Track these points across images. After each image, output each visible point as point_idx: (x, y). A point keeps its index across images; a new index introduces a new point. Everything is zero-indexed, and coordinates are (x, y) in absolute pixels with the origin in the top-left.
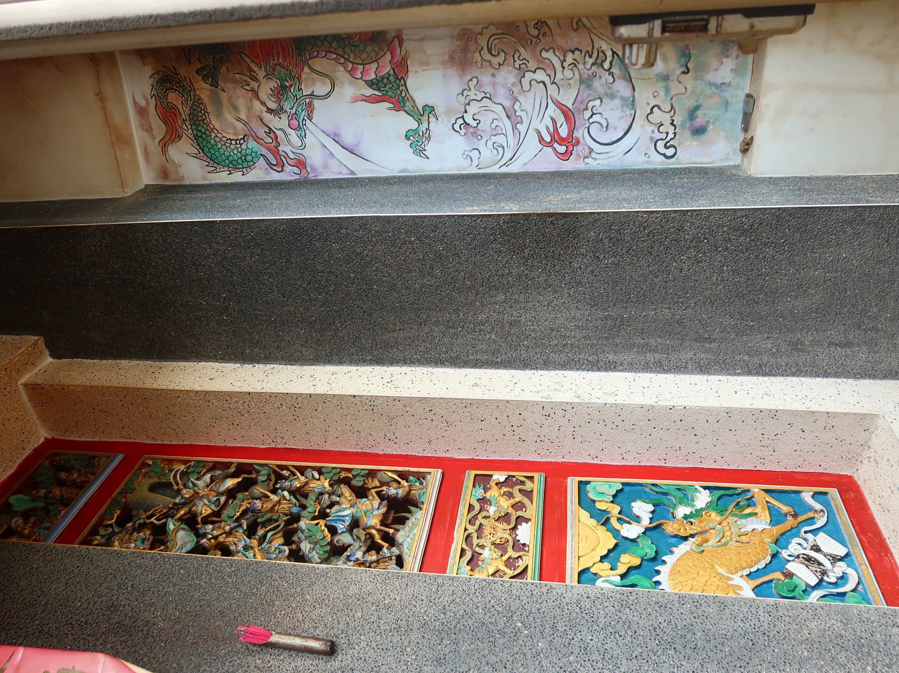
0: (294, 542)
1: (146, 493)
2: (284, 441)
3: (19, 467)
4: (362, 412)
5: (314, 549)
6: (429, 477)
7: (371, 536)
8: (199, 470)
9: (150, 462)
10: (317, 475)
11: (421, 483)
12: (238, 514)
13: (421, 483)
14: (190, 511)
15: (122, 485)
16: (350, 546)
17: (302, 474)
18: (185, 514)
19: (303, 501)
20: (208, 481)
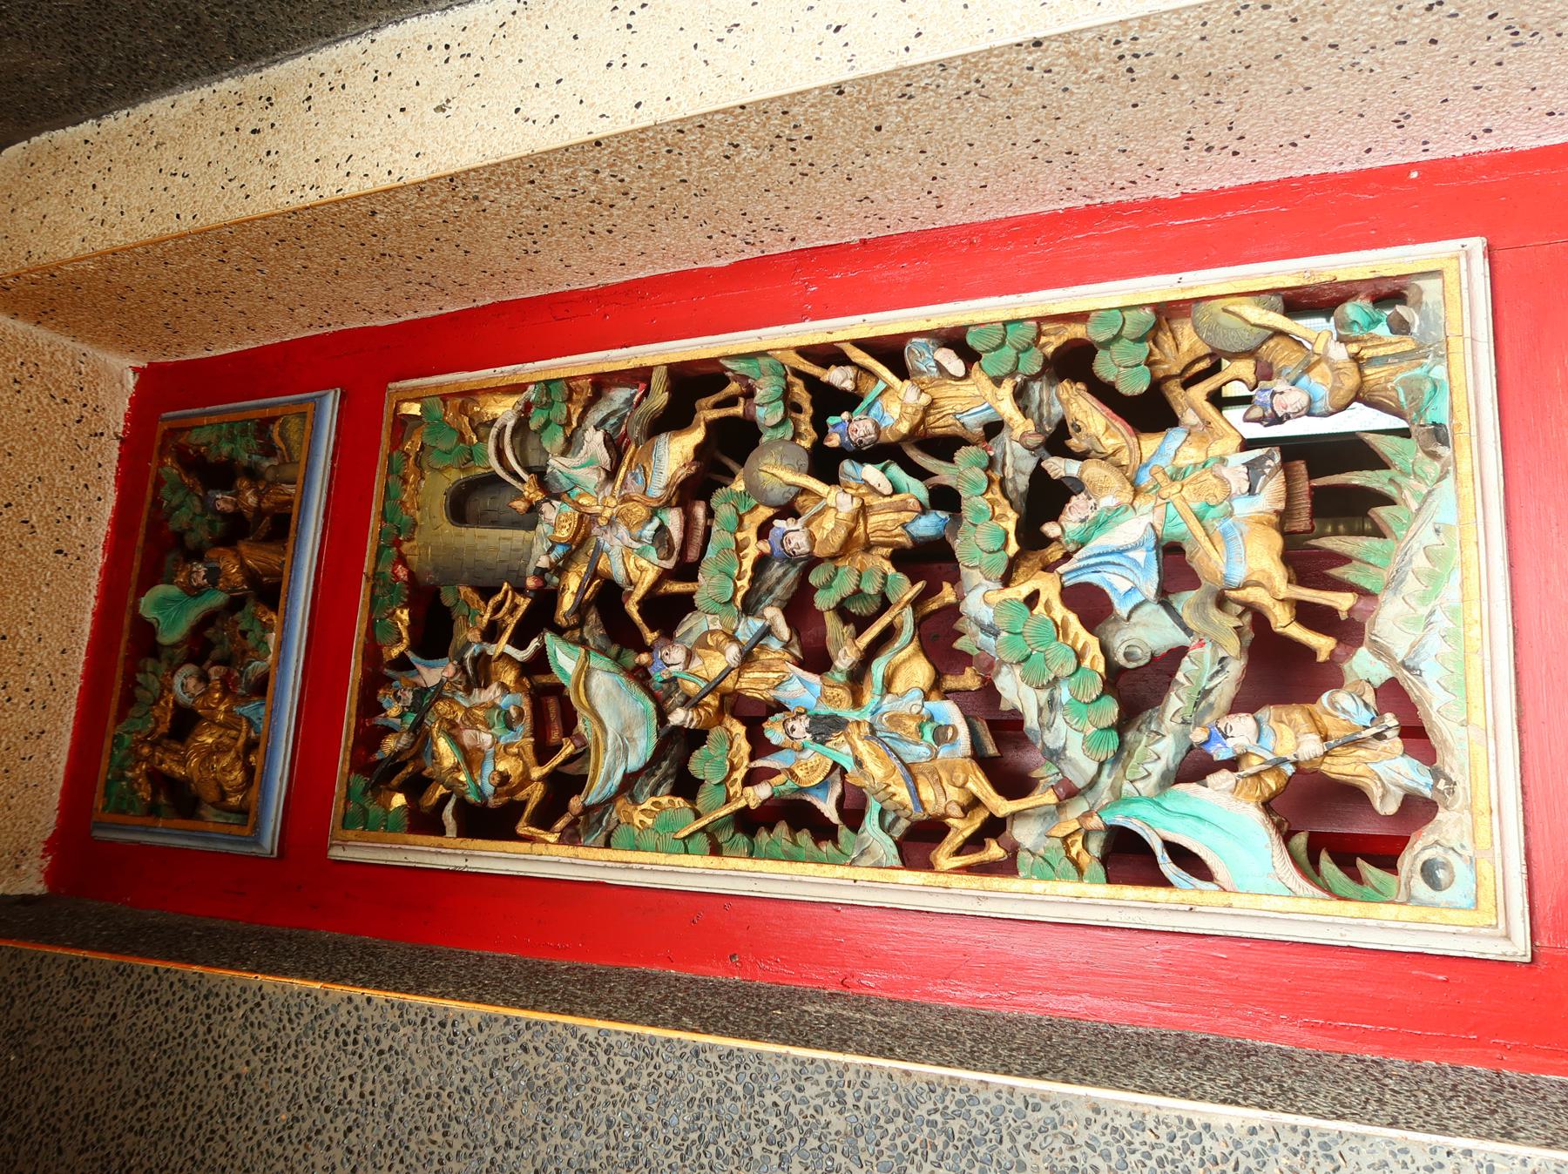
0: (965, 659)
1: (448, 530)
2: (786, 236)
3: (121, 482)
4: (1081, 92)
5: (1051, 703)
6: (1430, 287)
7: (1259, 619)
8: (559, 412)
9: (415, 409)
10: (955, 365)
11: (1400, 327)
12: (744, 584)
13: (1400, 327)
14: (594, 574)
15: (374, 523)
16: (1179, 653)
17: (902, 373)
18: (582, 590)
19: (945, 473)
20: (604, 457)
